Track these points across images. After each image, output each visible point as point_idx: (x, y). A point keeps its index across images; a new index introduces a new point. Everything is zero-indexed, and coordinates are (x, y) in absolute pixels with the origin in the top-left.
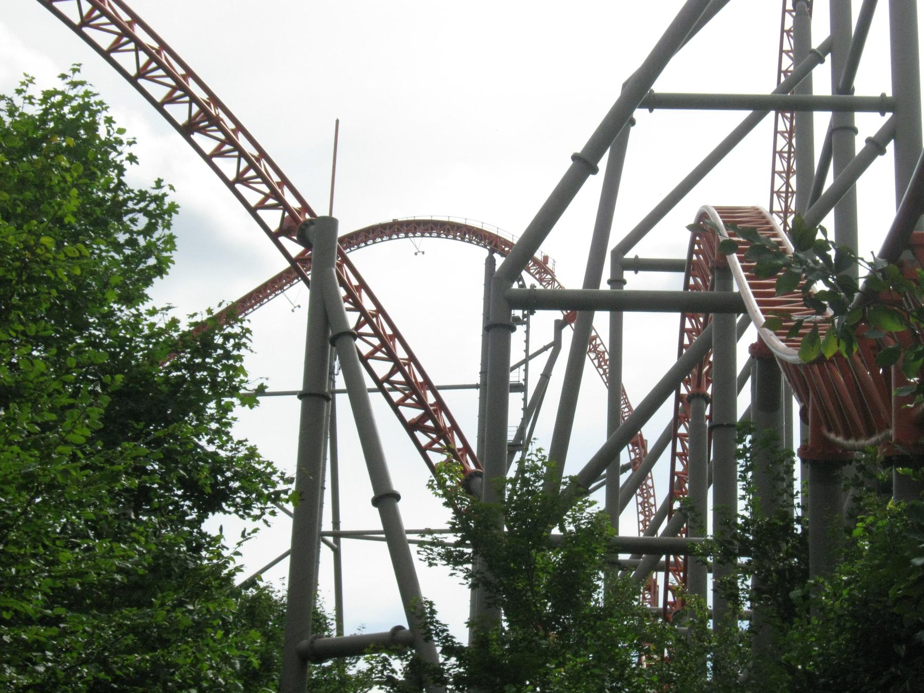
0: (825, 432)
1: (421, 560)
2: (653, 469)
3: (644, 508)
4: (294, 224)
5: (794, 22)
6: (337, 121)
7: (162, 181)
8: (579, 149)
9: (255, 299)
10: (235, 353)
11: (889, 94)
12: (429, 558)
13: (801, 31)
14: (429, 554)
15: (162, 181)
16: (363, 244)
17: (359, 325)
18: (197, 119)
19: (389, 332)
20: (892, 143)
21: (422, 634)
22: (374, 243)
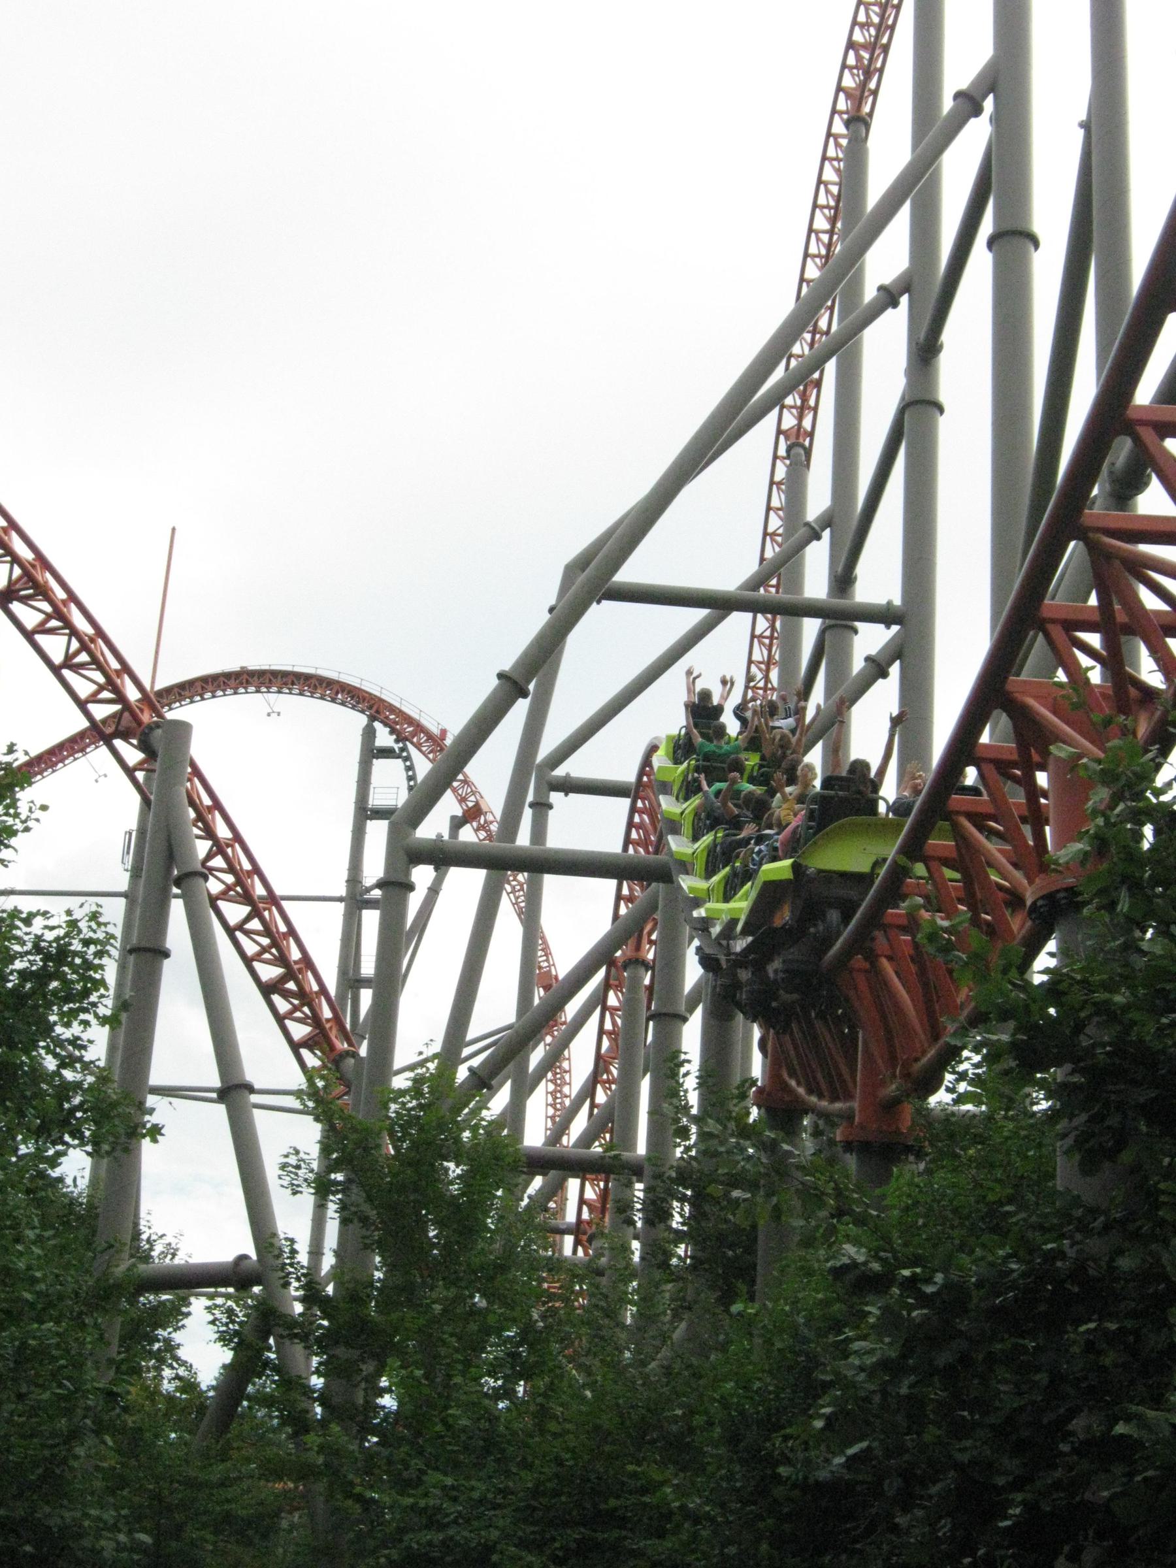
0: (786, 1076)
1: (282, 1186)
2: (571, 1045)
3: (555, 1098)
4: (134, 725)
5: (787, 473)
6: (174, 529)
7: (15, 745)
8: (507, 665)
9: (46, 763)
10: (97, 961)
11: (897, 601)
12: (293, 1185)
13: (795, 487)
14: (293, 1179)
15: (15, 745)
16: (198, 698)
17: (210, 856)
18: (17, 586)
19: (247, 866)
20: (897, 664)
21: (280, 1278)
22: (214, 697)
